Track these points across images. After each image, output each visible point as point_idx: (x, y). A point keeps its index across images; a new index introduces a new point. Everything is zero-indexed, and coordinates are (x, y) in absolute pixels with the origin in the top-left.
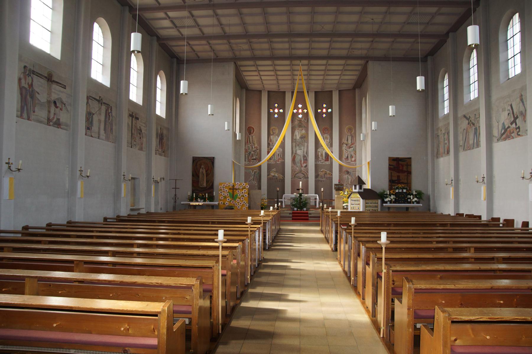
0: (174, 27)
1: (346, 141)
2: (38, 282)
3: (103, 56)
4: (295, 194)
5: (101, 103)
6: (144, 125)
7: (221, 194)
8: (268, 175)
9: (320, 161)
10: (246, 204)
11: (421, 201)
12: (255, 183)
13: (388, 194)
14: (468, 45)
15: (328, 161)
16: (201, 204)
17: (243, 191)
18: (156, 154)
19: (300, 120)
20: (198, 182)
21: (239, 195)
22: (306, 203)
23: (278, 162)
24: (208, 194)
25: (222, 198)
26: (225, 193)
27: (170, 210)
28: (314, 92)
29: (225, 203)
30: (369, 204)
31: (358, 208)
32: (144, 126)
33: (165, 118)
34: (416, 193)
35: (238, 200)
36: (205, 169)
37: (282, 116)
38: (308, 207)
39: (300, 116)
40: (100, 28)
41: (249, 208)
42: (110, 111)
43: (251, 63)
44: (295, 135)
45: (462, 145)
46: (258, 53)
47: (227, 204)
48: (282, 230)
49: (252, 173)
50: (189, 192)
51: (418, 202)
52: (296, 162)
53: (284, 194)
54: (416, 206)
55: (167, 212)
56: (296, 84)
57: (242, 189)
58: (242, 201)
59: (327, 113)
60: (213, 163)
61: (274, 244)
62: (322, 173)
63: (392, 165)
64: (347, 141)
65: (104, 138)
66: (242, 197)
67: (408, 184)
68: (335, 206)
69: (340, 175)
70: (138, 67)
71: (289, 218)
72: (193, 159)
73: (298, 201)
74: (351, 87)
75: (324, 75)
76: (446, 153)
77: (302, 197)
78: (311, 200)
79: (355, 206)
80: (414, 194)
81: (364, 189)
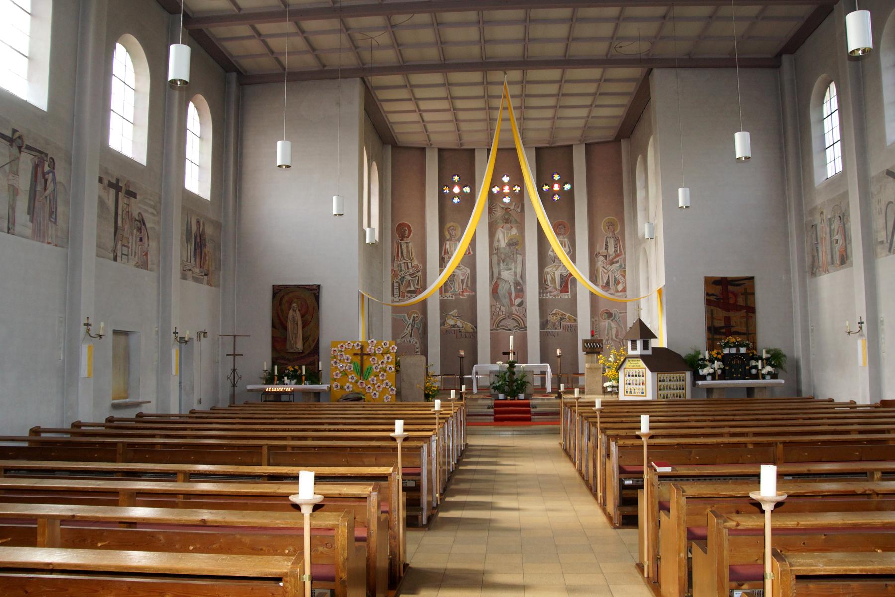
0: (256, 36)
1: (604, 248)
2: (61, 527)
3: (134, 107)
4: (498, 362)
5: (20, 148)
6: (151, 210)
7: (336, 367)
8: (442, 324)
9: (551, 292)
10: (390, 387)
11: (781, 372)
12: (415, 341)
13: (707, 358)
14: (849, 51)
15: (568, 292)
16: (288, 389)
17: (384, 358)
18: (184, 277)
19: (506, 209)
20: (285, 340)
21: (376, 368)
22: (523, 382)
23: (461, 297)
24: (306, 366)
25: (336, 375)
26: (344, 365)
27: (224, 404)
28: (534, 149)
29: (345, 387)
30: (667, 381)
31: (643, 393)
32: (152, 214)
33: (209, 199)
34: (769, 356)
35: (373, 380)
36: (299, 311)
37: (469, 200)
38: (529, 389)
39: (507, 200)
40: (127, 53)
41: (398, 394)
42: (47, 168)
43: (398, 79)
44: (496, 239)
45: (885, 240)
46: (412, 55)
47: (348, 387)
48: (471, 450)
49: (407, 319)
50: (265, 364)
51: (774, 376)
52: (500, 295)
53: (477, 364)
54: (771, 383)
55: (211, 409)
56: (495, 130)
57: (382, 354)
58: (383, 380)
59: (561, 192)
60: (317, 298)
61: (461, 468)
62: (555, 318)
63: (712, 295)
64: (605, 249)
65: (29, 232)
66: (382, 372)
67: (750, 335)
68: (586, 387)
69: (593, 320)
70: (137, 80)
71: (489, 417)
72: (274, 291)
73: (507, 380)
74: (610, 134)
75: (555, 107)
76: (838, 261)
77: (515, 369)
78: (534, 376)
79: (635, 386)
80: (764, 357)
81: (653, 348)
